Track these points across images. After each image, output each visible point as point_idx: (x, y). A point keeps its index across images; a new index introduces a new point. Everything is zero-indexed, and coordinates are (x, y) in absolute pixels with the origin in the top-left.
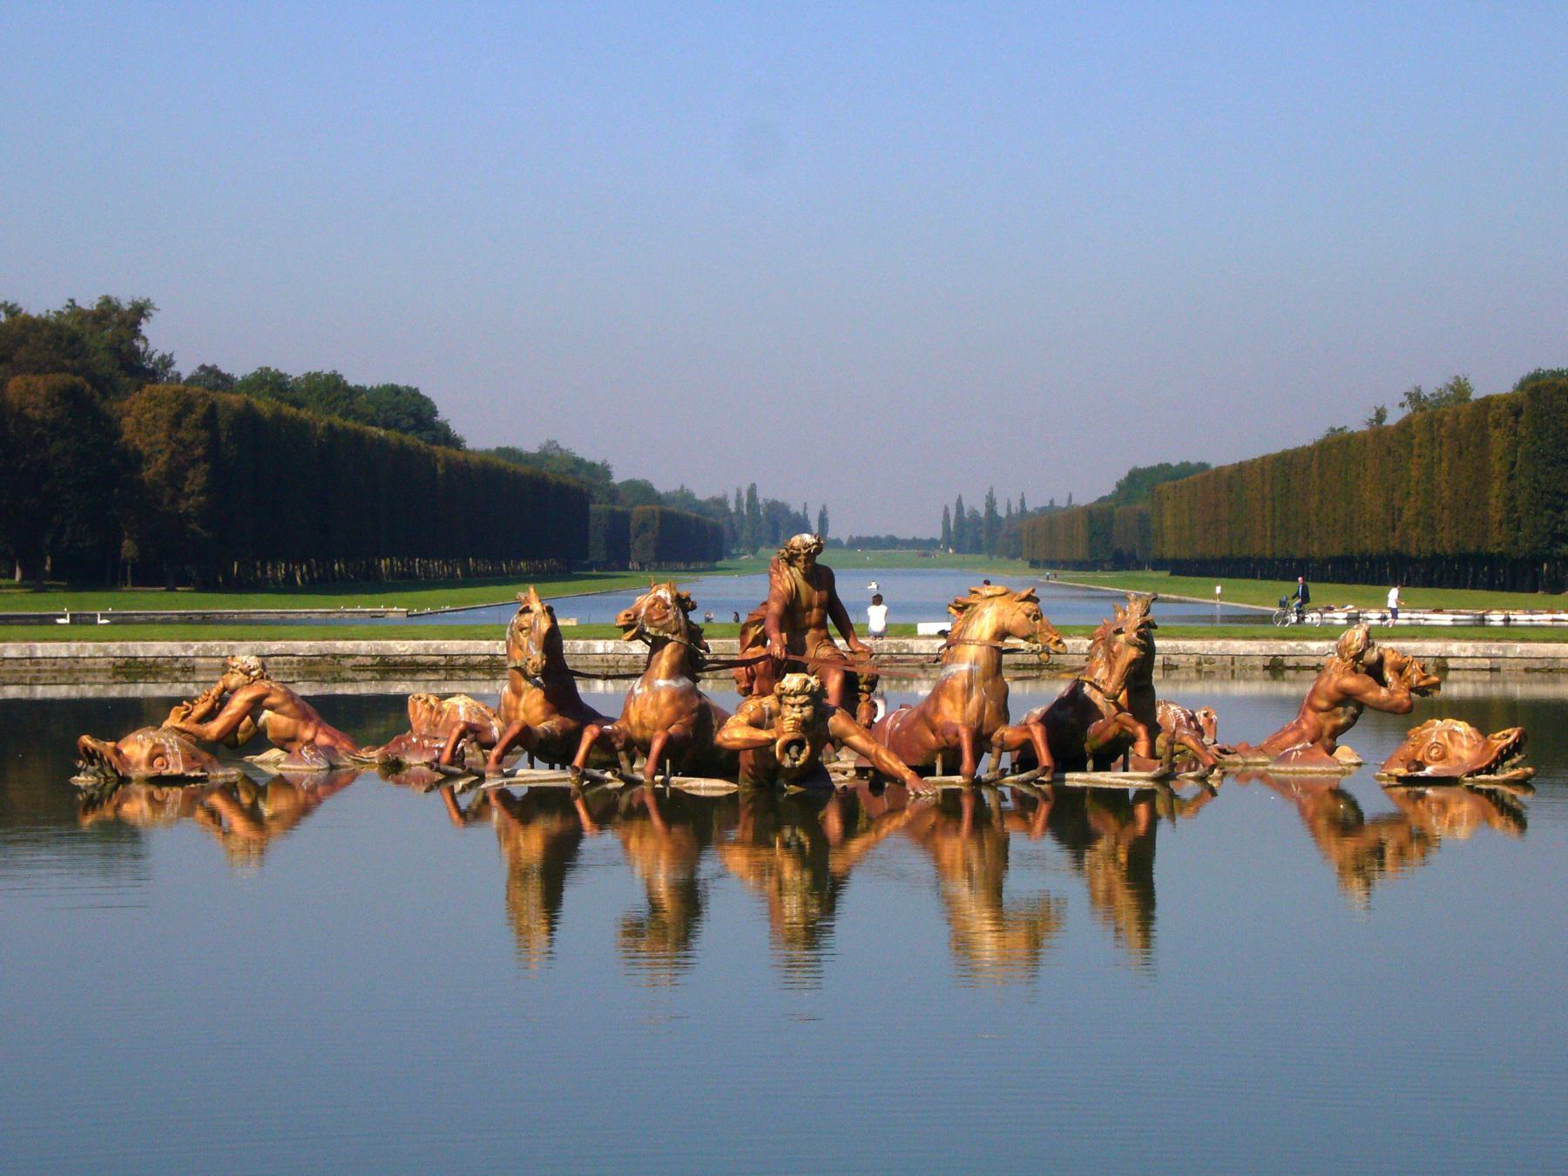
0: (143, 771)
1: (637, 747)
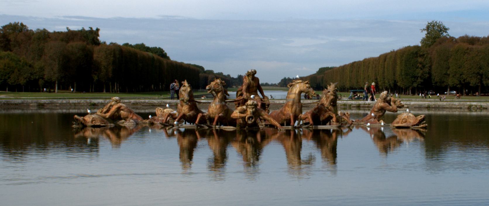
0: (90, 124)
1: (211, 120)
